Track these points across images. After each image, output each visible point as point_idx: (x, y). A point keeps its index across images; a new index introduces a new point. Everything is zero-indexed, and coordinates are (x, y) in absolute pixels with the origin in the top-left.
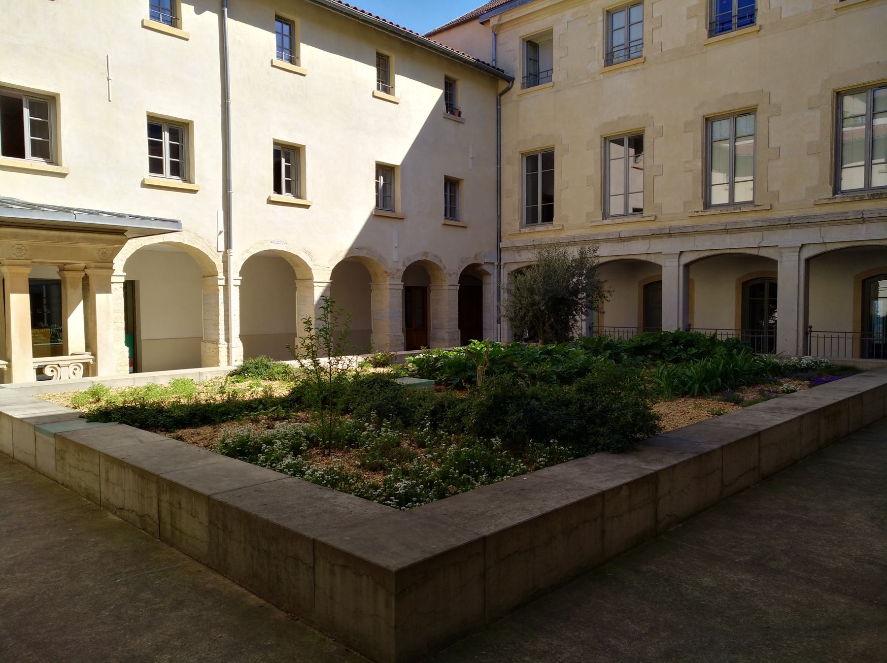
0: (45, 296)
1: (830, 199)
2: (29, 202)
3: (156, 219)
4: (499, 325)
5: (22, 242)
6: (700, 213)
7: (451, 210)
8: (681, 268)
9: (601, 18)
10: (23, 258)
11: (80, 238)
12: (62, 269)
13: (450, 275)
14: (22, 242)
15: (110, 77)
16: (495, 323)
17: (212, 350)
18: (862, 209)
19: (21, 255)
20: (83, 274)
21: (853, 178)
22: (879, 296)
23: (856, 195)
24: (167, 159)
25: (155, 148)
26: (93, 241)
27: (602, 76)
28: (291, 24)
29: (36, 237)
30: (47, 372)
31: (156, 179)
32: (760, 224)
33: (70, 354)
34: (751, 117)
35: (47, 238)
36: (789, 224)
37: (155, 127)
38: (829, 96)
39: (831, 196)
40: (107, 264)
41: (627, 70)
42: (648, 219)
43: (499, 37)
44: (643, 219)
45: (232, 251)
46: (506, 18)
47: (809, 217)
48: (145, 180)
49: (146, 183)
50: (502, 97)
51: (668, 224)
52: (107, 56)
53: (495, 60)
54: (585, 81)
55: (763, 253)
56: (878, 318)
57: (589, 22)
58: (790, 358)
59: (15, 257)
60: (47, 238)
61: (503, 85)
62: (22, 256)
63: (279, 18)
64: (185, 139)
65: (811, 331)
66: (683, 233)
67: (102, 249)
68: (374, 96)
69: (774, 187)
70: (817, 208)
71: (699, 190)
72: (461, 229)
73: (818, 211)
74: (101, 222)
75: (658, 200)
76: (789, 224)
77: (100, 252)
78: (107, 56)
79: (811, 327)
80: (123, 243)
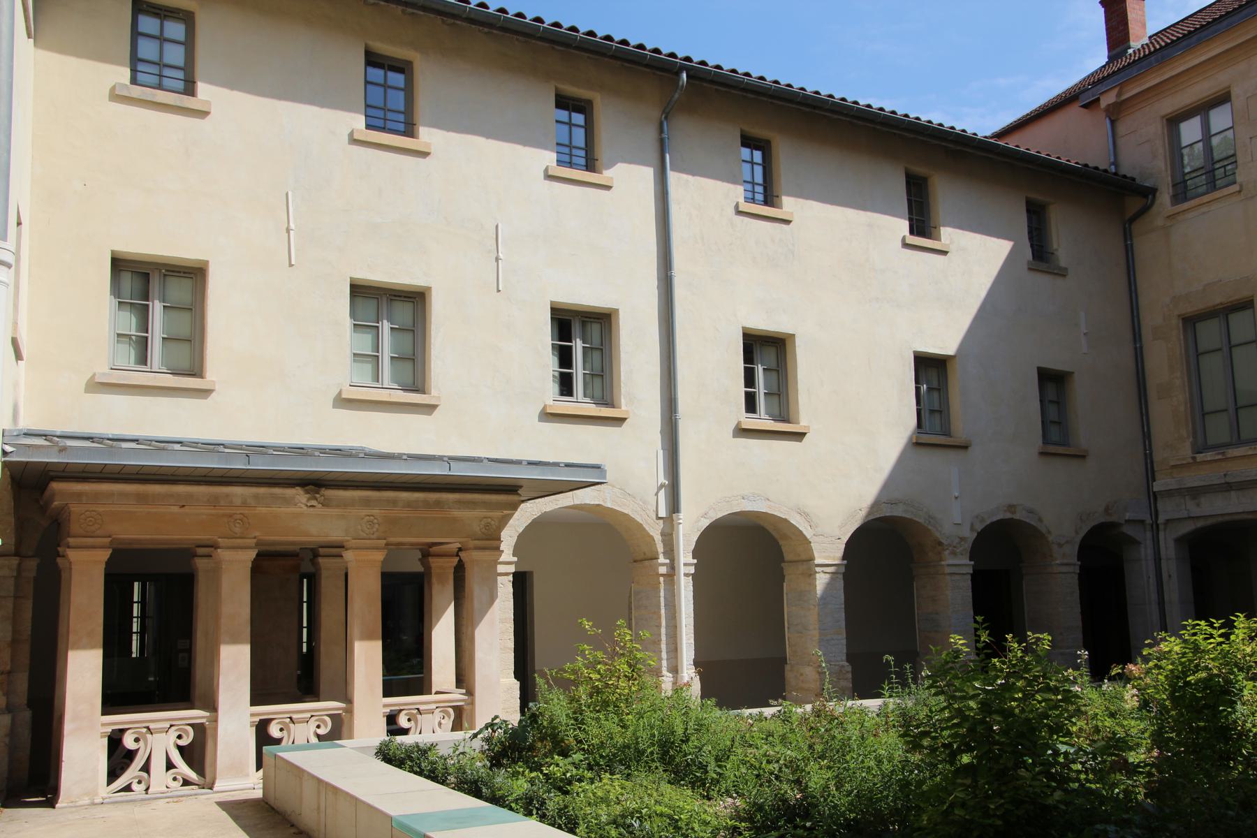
60: (409, 505)
77: (483, 523)
78: (497, 227)
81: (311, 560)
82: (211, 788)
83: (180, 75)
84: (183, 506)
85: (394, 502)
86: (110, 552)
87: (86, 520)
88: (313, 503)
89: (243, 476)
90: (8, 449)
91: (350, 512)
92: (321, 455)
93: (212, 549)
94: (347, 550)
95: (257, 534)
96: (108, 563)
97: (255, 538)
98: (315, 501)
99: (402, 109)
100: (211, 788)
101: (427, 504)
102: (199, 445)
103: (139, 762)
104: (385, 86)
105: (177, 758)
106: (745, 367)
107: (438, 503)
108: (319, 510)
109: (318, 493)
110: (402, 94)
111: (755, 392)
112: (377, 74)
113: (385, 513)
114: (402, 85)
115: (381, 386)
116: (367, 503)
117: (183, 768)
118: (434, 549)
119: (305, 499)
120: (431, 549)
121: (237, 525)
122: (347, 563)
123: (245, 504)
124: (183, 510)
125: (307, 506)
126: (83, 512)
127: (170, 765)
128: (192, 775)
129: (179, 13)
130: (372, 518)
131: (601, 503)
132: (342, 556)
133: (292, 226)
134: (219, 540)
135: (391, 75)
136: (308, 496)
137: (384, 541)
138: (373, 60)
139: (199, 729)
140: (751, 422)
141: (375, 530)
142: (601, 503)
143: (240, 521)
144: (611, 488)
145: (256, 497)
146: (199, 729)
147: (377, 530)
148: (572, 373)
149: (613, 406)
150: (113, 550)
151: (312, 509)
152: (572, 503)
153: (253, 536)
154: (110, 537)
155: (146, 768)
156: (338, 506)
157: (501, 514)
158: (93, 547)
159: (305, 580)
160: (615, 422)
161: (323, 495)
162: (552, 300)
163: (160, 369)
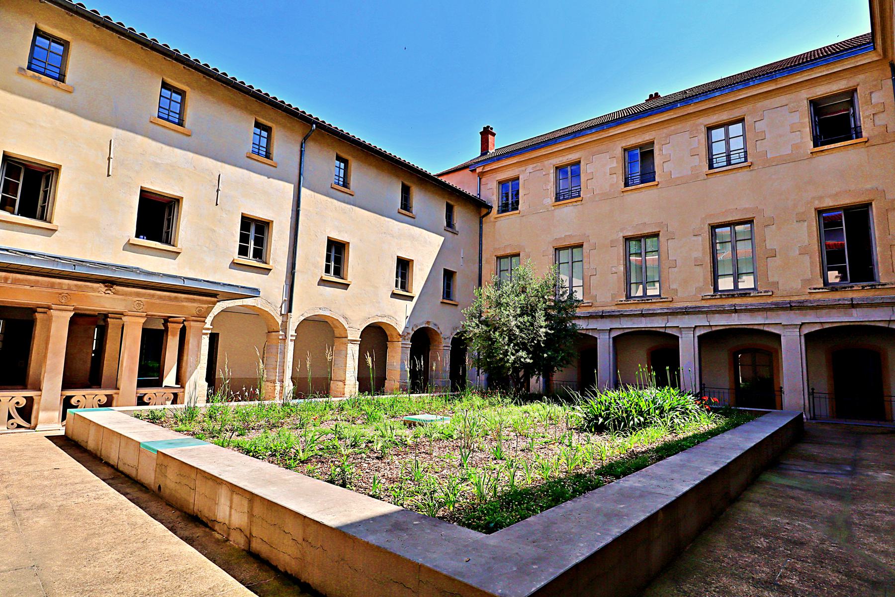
0: (95, 341)
1: (712, 296)
2: (894, 26)
3: (242, 287)
4: (478, 377)
6: (623, 302)
7: (448, 294)
8: (611, 340)
9: (552, 171)
12: (166, 320)
13: (445, 339)
15: (220, 188)
16: (476, 375)
17: (269, 387)
18: (734, 303)
20: (182, 325)
21: (725, 284)
23: (729, 294)
24: (252, 245)
25: (244, 238)
26: (194, 301)
27: (553, 208)
28: (346, 162)
30: (146, 399)
31: (243, 260)
32: (666, 311)
33: (163, 386)
34: (518, 258)
35: (160, 298)
36: (790, 307)
37: (246, 222)
38: (706, 228)
39: (712, 293)
40: (201, 317)
41: (570, 204)
42: (586, 304)
43: (482, 180)
44: (661, 300)
45: (292, 314)
46: (487, 168)
47: (699, 307)
50: (484, 219)
51: (601, 309)
52: (219, 175)
53: (479, 194)
54: (541, 211)
55: (669, 331)
57: (544, 173)
59: (135, 310)
60: (160, 298)
61: (484, 211)
63: (339, 158)
64: (266, 234)
65: (704, 387)
66: (611, 316)
68: (399, 212)
69: (674, 286)
70: (703, 302)
71: (623, 286)
72: (454, 307)
73: (704, 303)
75: (593, 292)
76: (790, 307)
78: (219, 175)
79: (704, 385)
80: (215, 303)
85: (153, 296)
101: (170, 299)
105: (14, 414)
110: (179, 105)
112: (167, 93)
116: (138, 295)
117: (19, 420)
133: (112, 156)
139: (30, 400)
140: (243, 260)
145: (76, 285)
146: (30, 400)
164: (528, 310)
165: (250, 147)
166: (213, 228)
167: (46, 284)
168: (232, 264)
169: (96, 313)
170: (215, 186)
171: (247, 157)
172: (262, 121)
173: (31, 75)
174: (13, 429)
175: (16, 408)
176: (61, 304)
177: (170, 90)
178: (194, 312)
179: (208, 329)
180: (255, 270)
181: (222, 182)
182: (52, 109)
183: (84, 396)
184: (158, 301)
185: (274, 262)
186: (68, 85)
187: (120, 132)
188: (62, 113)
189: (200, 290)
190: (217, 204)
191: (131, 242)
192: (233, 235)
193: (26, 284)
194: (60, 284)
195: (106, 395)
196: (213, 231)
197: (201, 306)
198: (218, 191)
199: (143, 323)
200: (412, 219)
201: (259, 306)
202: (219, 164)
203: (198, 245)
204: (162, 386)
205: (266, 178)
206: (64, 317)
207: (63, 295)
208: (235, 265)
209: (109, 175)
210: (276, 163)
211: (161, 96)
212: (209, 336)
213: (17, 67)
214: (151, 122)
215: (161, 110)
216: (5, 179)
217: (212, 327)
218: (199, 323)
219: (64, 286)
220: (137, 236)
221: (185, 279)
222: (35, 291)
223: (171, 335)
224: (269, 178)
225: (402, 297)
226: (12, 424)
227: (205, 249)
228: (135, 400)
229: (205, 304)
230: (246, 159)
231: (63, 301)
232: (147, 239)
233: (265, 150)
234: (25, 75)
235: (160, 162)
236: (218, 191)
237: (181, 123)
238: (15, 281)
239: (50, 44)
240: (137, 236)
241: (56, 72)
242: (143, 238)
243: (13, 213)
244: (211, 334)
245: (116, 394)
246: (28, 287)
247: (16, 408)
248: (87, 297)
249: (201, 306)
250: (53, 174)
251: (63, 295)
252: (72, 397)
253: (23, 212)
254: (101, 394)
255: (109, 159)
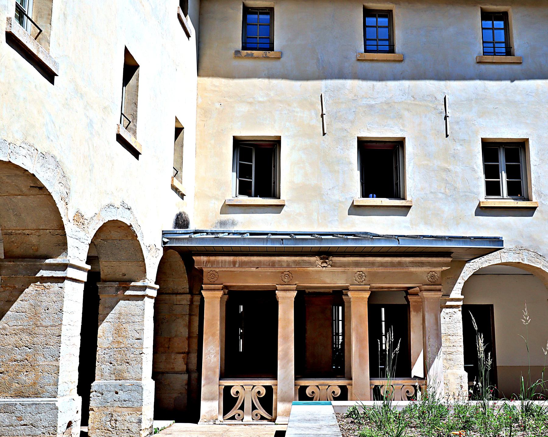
5: (362, 269)
10: (363, 284)
11: (410, 262)
14: (362, 269)
19: (361, 281)
22: (367, 44)
26: (422, 264)
29: (373, 264)
31: (494, 202)
33: (412, 377)
48: (481, 203)
49: (482, 205)
52: (445, 98)
56: (503, 171)
58: (386, 400)
60: (382, 265)
62: (362, 282)
67: (431, 272)
74: (441, 245)
77: (429, 275)
78: (445, 98)
81: (405, 297)
82: (274, 422)
83: (387, 43)
84: (258, 268)
85: (373, 264)
86: (296, 293)
87: (210, 275)
88: (325, 265)
89: (398, 251)
90: (166, 240)
91: (348, 270)
92: (373, 238)
93: (347, 291)
94: (349, 291)
95: (297, 282)
96: (369, 299)
97: (296, 285)
98: (326, 264)
99: (503, 40)
100: (274, 422)
101: (393, 265)
102: (245, 236)
103: (238, 404)
104: (493, 29)
105: (257, 404)
106: (506, 165)
107: (400, 264)
108: (330, 269)
109: (328, 259)
110: (503, 31)
111: (499, 181)
112: (489, 24)
113: (369, 270)
114: (502, 27)
115: (502, 198)
116: (357, 264)
117: (262, 412)
118: (410, 291)
119: (321, 263)
120: (408, 291)
121: (286, 278)
122: (350, 299)
123: (288, 266)
124: (257, 270)
125: (322, 267)
126: (209, 271)
127: (254, 408)
128: (265, 415)
129: (266, 10)
130: (361, 272)
131: (521, 261)
132: (348, 295)
133: (324, 112)
134: (277, 286)
135: (380, 20)
136: (321, 261)
137: (369, 286)
138: (486, 16)
139: (269, 389)
140: (494, 202)
141: (363, 279)
142: (520, 261)
143: (288, 276)
144: (527, 251)
145: (294, 262)
146: (269, 389)
147: (365, 280)
148: (507, 179)
149: (404, 199)
150: (371, 292)
151: (324, 268)
152: (501, 262)
153: (295, 284)
154: (222, 284)
155: (242, 408)
156: (340, 267)
157: (441, 269)
158: (214, 290)
159: (383, 309)
160: (512, 209)
161: (332, 260)
162: (482, 137)
163: (507, 197)
164: (444, 185)
165: (480, 48)
166: (446, 165)
167: (268, 264)
168: (479, 209)
169: (331, 291)
170: (441, 113)
171: (478, 63)
172: (491, 8)
173: (245, 54)
174: (257, 420)
175: (258, 397)
176: (284, 283)
177: (374, 16)
178: (426, 278)
179: (458, 300)
180: (262, 209)
181: (449, 104)
182: (266, 81)
183: (317, 386)
184: (381, 270)
185: (540, 195)
186: (276, 52)
187: (329, 82)
188: (274, 82)
189: (418, 250)
190: (447, 136)
191: (355, 204)
192: (474, 170)
193: (251, 265)
194: (279, 261)
195: (340, 386)
196: (447, 170)
197: (434, 269)
198: (446, 118)
199: (369, 298)
200: (398, 66)
201: (526, 262)
202: (442, 83)
203: (431, 192)
204: (411, 377)
205: (508, 82)
206: (289, 298)
207: (285, 273)
208: (482, 210)
209: (324, 134)
210: (521, 58)
211: (483, 29)
212: (461, 309)
213: (234, 52)
214: (358, 60)
215: (486, 45)
216: (240, 163)
217: (463, 297)
218: (433, 293)
219: (283, 264)
220: (365, 194)
221: (397, 238)
222: (260, 272)
223: (415, 311)
224: (512, 81)
225: (494, 212)
226: (257, 415)
227: (440, 195)
228: (368, 392)
229: (435, 267)
230: (477, 65)
231: (286, 280)
232: (377, 197)
233: (503, 45)
234: (241, 57)
235: (373, 103)
236: (446, 118)
237: (509, 52)
238: (242, 264)
239: (493, 23)
240: (365, 194)
241: (385, 45)
242: (373, 197)
243: (250, 195)
244: (463, 306)
245: (349, 385)
246: (254, 269)
247: (258, 398)
248: (307, 273)
249: (434, 269)
250: (399, 147)
251: (285, 273)
252: (231, 387)
253: (260, 193)
254: (335, 384)
255: (322, 116)
